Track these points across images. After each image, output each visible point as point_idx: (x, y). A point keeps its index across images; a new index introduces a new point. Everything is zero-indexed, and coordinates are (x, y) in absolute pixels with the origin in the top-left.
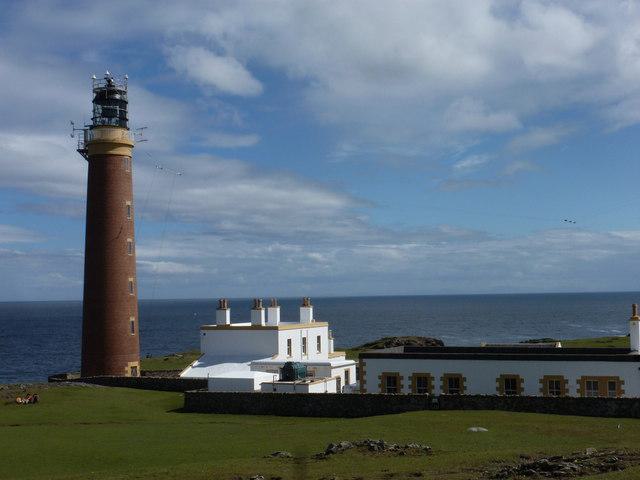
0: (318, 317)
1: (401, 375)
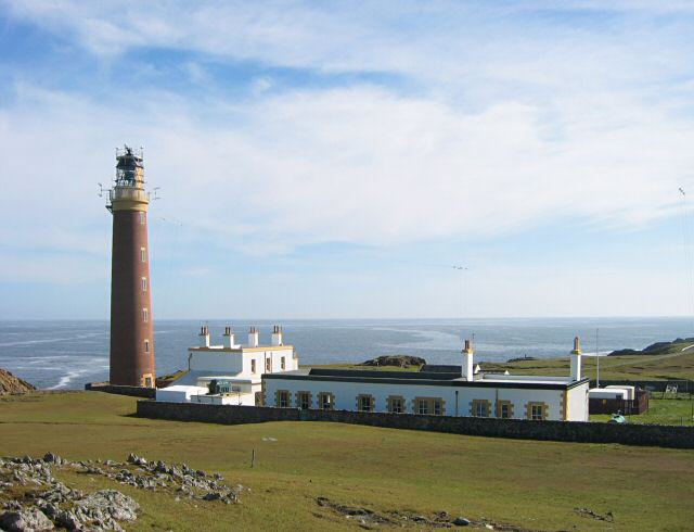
0: (286, 343)
1: (443, 400)
